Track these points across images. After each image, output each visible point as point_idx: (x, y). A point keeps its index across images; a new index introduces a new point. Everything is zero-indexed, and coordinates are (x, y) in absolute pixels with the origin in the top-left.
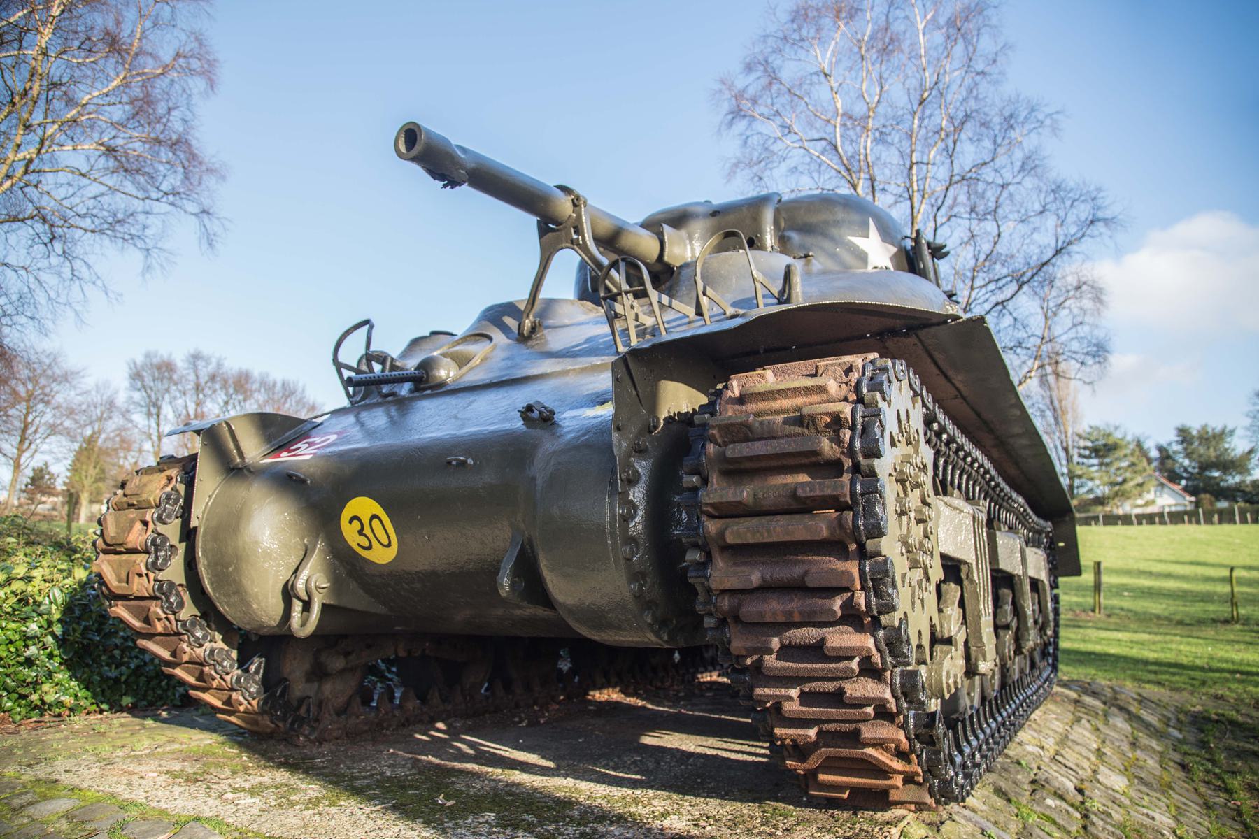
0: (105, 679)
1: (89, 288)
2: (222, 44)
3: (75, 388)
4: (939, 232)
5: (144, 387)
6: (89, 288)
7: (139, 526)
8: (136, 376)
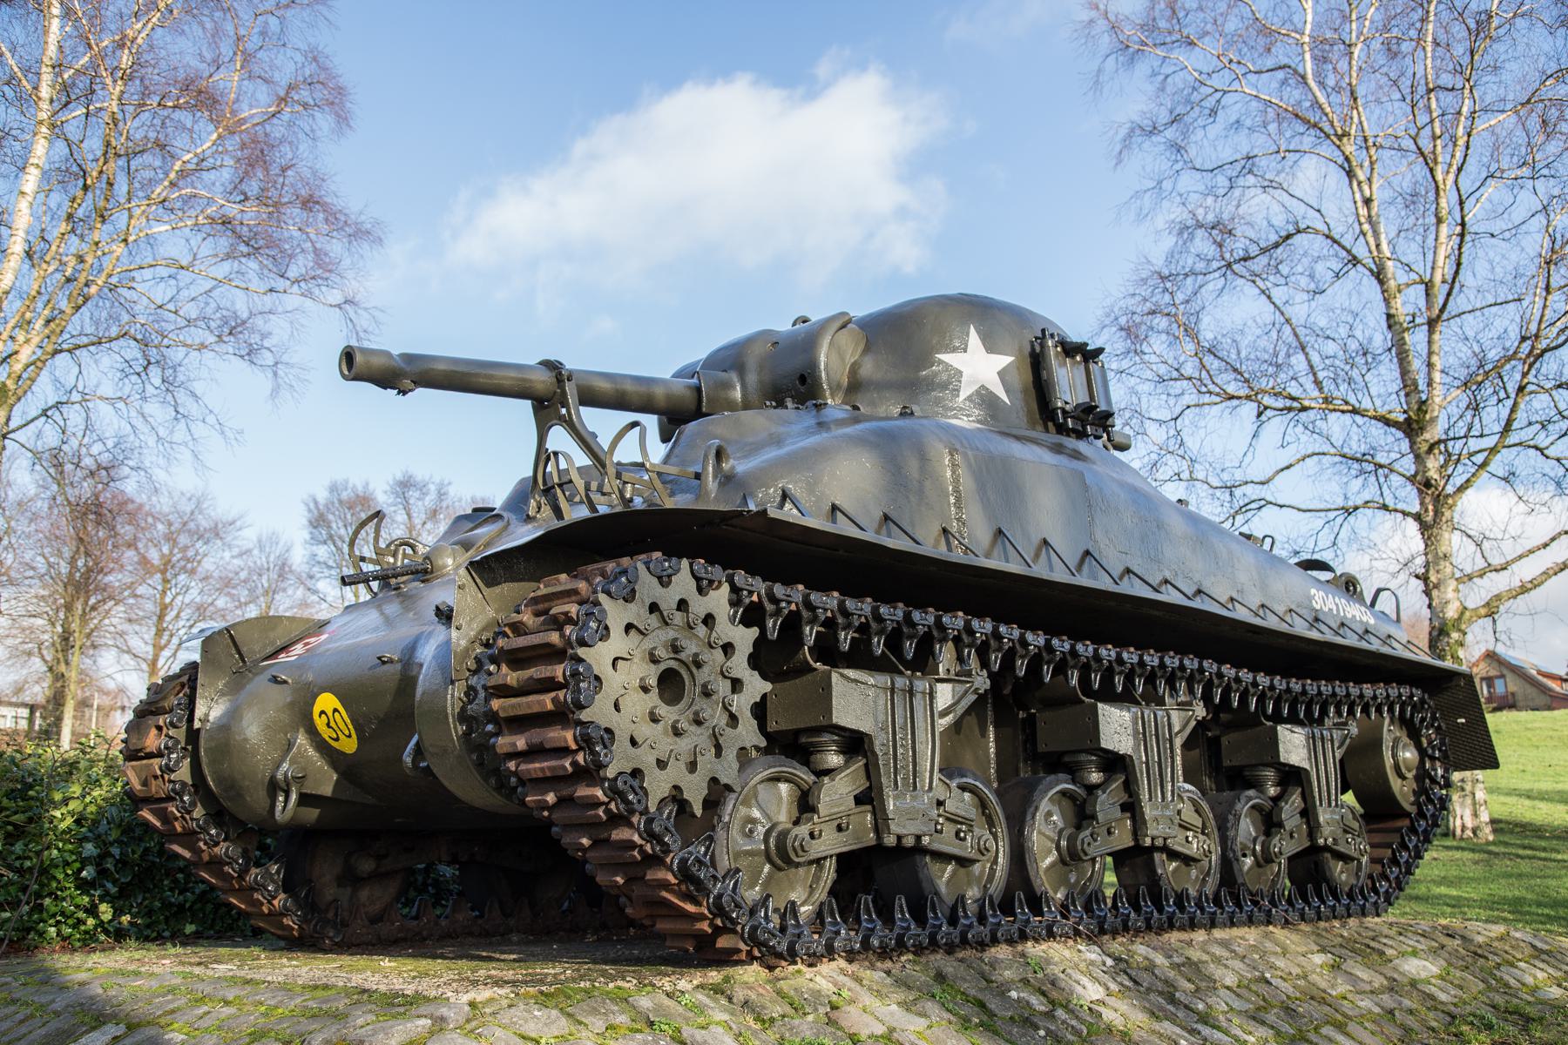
0: (166, 905)
1: (199, 429)
2: (347, 65)
3: (230, 547)
4: (1467, 206)
5: (331, 537)
6: (199, 429)
7: (154, 731)
8: (319, 521)
